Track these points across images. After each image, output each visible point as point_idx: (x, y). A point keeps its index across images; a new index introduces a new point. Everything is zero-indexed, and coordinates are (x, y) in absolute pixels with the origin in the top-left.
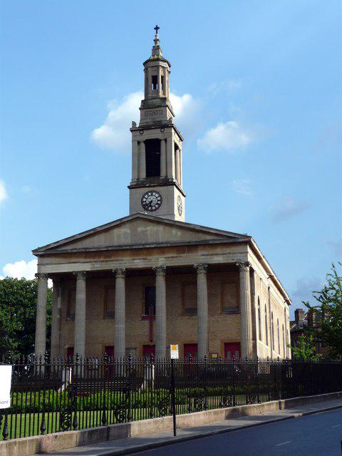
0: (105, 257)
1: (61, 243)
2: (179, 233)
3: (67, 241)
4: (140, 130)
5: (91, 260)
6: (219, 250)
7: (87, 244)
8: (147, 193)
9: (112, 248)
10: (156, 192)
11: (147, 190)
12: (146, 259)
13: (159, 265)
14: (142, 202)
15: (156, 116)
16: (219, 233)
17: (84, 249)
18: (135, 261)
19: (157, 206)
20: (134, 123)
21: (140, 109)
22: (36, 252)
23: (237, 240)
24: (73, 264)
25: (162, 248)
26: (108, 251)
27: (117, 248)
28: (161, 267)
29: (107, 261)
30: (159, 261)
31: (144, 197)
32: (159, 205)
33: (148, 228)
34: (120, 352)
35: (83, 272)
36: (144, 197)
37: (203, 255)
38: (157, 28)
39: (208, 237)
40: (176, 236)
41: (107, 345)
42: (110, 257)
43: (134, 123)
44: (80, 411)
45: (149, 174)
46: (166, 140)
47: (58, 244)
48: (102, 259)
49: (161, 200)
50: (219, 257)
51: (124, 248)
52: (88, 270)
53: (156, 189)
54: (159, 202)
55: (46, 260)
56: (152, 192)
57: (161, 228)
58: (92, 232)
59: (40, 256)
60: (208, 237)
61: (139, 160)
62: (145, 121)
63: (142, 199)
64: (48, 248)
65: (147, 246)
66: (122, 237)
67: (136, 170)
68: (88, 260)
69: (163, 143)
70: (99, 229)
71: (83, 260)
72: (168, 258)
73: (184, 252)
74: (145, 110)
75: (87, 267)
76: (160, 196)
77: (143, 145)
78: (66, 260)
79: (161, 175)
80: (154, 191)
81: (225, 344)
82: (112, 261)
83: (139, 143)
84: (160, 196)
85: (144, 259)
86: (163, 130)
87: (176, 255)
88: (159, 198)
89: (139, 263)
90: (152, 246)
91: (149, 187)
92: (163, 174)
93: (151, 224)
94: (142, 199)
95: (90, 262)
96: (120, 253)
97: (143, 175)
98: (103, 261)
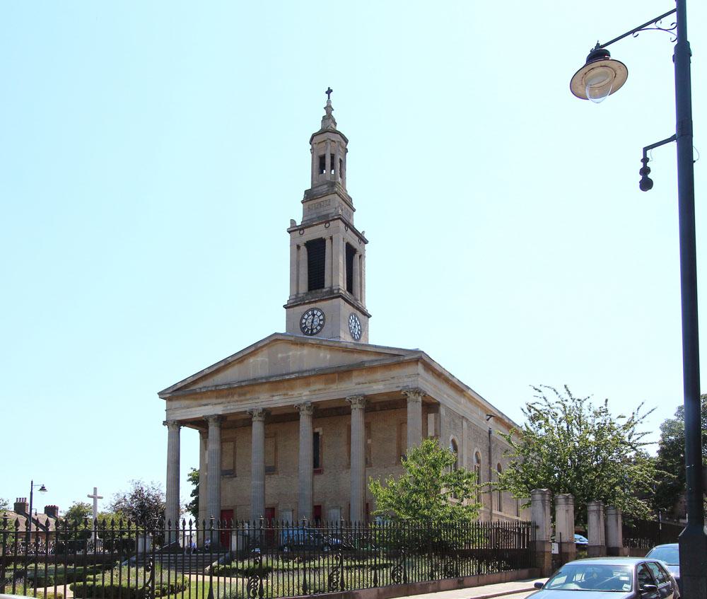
0: (240, 395)
1: (189, 381)
3: (183, 384)
4: (300, 230)
5: (224, 400)
6: (379, 375)
7: (219, 379)
8: (307, 312)
9: (247, 383)
10: (319, 310)
11: (307, 307)
12: (287, 394)
13: (302, 402)
14: (301, 324)
15: (322, 209)
16: (378, 350)
18: (275, 398)
19: (319, 328)
20: (293, 222)
21: (303, 202)
22: (161, 394)
23: (401, 359)
24: (203, 408)
25: (305, 377)
26: (242, 387)
27: (251, 383)
28: (305, 404)
29: (241, 401)
30: (302, 395)
31: (303, 318)
32: (322, 326)
33: (290, 353)
34: (379, 507)
36: (303, 318)
38: (329, 92)
39: (365, 358)
41: (316, 505)
42: (244, 394)
43: (293, 222)
44: (379, 557)
45: (310, 288)
46: (331, 238)
48: (236, 398)
49: (324, 320)
50: (379, 385)
51: (260, 381)
52: (220, 413)
54: (321, 323)
55: (176, 404)
56: (312, 310)
58: (223, 364)
59: (168, 399)
60: (365, 358)
61: (298, 270)
62: (309, 217)
63: (301, 320)
64: (175, 388)
65: (287, 377)
66: (257, 369)
67: (295, 283)
68: (220, 401)
69: (328, 243)
70: (230, 360)
71: (215, 401)
72: (315, 391)
73: (333, 381)
74: (308, 203)
75: (219, 410)
76: (323, 314)
78: (193, 402)
79: (326, 286)
80: (316, 309)
82: (248, 400)
83: (298, 247)
86: (327, 225)
88: (321, 317)
89: (277, 400)
90: (293, 376)
91: (310, 303)
92: (327, 284)
93: (293, 347)
94: (301, 320)
95: (222, 403)
96: (257, 388)
97: (304, 287)
98: (237, 401)
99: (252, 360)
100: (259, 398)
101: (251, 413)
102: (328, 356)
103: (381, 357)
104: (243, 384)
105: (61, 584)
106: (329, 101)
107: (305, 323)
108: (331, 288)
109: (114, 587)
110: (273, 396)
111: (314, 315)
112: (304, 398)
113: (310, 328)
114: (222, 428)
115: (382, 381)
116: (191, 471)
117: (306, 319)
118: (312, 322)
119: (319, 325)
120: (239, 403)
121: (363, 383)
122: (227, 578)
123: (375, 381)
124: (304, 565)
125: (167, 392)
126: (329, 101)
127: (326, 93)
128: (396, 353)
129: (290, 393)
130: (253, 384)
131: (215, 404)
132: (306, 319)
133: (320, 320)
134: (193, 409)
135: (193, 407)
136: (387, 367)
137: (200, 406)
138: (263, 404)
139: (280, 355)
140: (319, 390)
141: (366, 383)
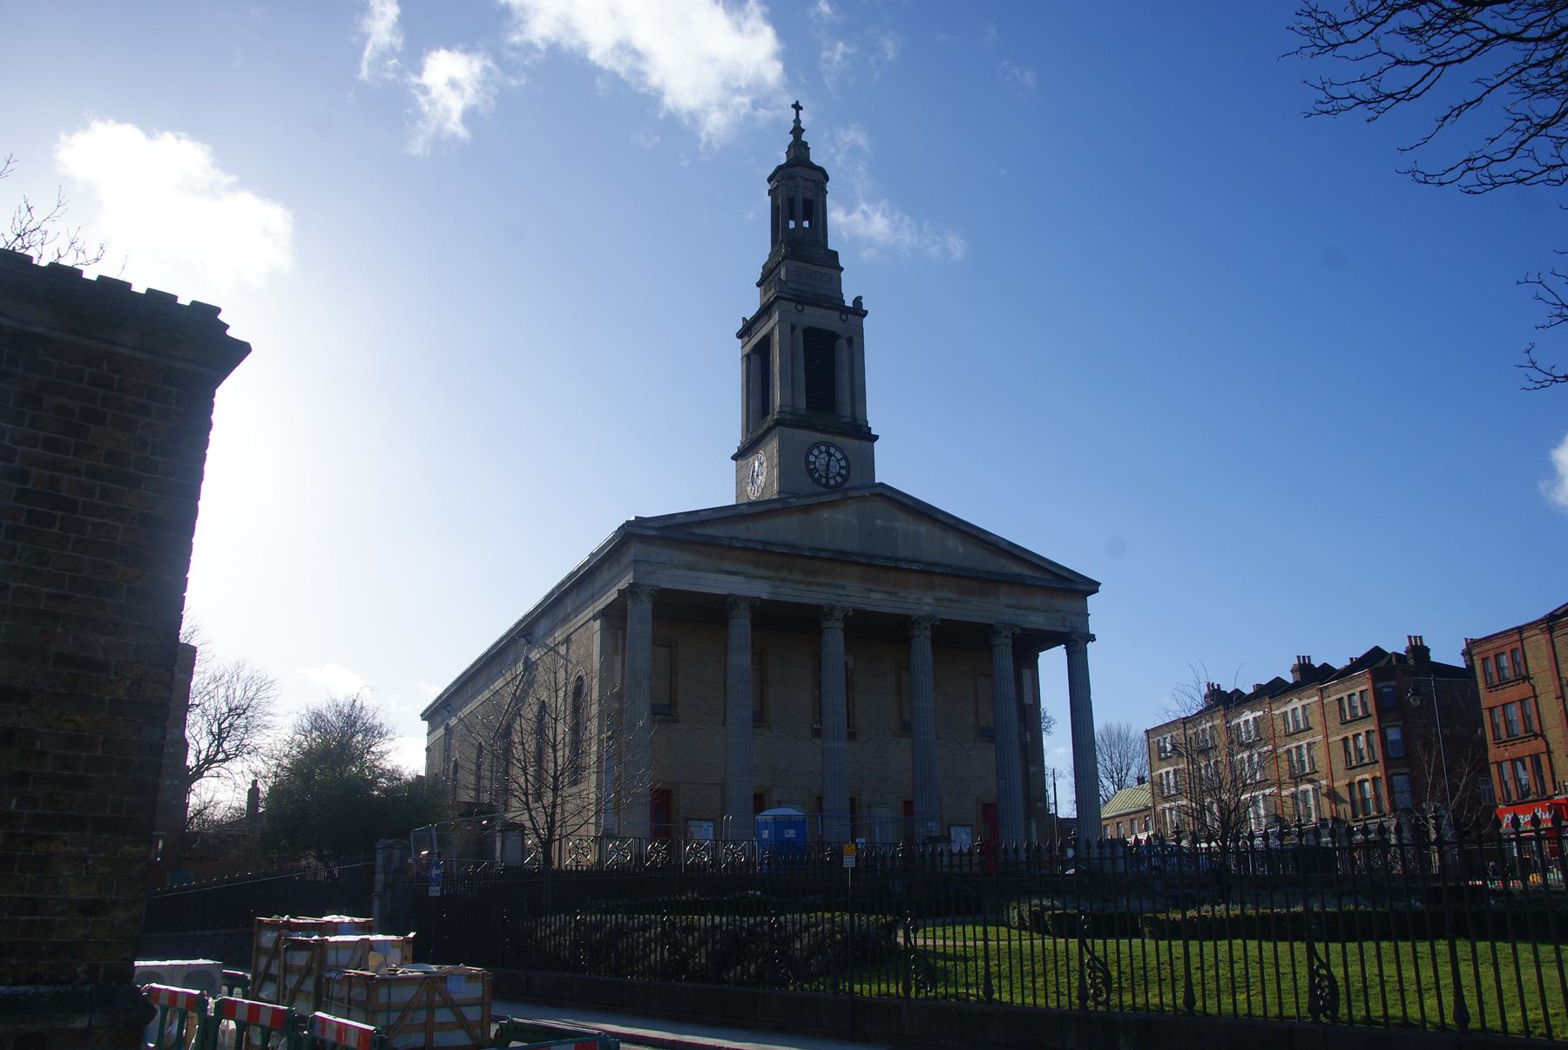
2: (961, 549)
8: (817, 445)
10: (838, 448)
11: (817, 437)
12: (896, 594)
14: (808, 462)
16: (1042, 563)
17: (759, 542)
18: (873, 595)
19: (839, 479)
25: (929, 572)
29: (809, 584)
30: (922, 602)
35: (751, 599)
36: (809, 452)
37: (1011, 607)
40: (956, 551)
46: (850, 341)
47: (696, 518)
49: (848, 468)
51: (854, 558)
53: (837, 439)
56: (828, 445)
57: (924, 528)
60: (1016, 569)
68: (765, 573)
75: (760, 589)
77: (799, 334)
80: (835, 446)
81: (984, 805)
82: (820, 585)
83: (793, 328)
84: (845, 458)
85: (891, 593)
87: (954, 596)
88: (843, 463)
89: (879, 600)
90: (915, 567)
91: (822, 432)
92: (845, 410)
97: (802, 403)
99: (826, 514)
100: (843, 587)
101: (832, 609)
102: (961, 549)
103: (1039, 575)
104: (822, 555)
105: (1224, 939)
106: (797, 121)
107: (814, 463)
108: (853, 416)
109: (1467, 937)
110: (871, 590)
111: (830, 455)
112: (926, 608)
113: (823, 474)
114: (756, 624)
115: (1044, 611)
116: (1124, 726)
117: (816, 457)
118: (828, 465)
119: (839, 474)
120: (803, 587)
121: (1015, 607)
122: (1160, 942)
123: (1035, 609)
124: (944, 931)
125: (650, 524)
126: (797, 121)
127: (793, 106)
128: (1066, 575)
129: (900, 594)
130: (841, 559)
131: (754, 577)
132: (838, 461)
133: (841, 467)
134: (702, 575)
135: (702, 570)
136: (1046, 589)
137: (720, 571)
138: (850, 599)
139: (879, 522)
140: (951, 600)
141: (1020, 608)
